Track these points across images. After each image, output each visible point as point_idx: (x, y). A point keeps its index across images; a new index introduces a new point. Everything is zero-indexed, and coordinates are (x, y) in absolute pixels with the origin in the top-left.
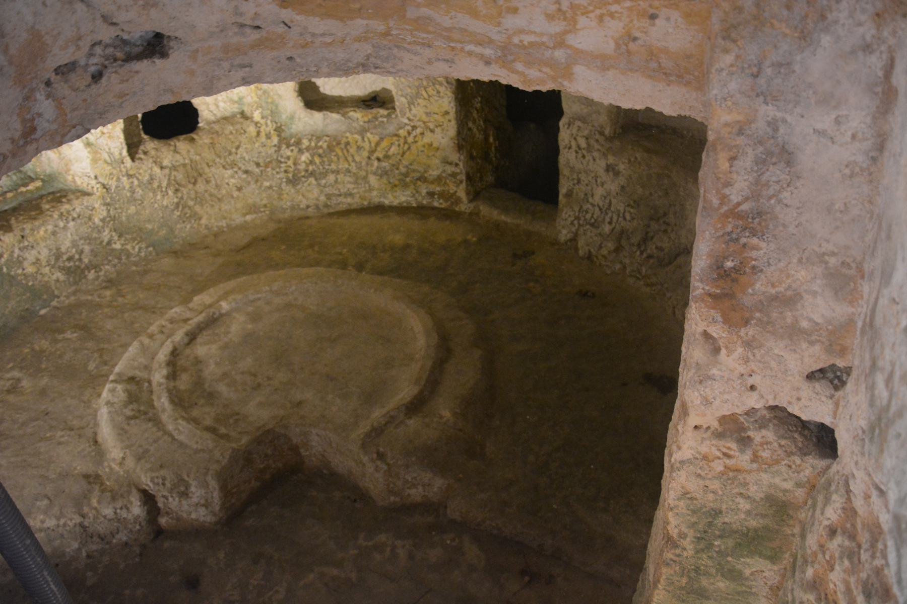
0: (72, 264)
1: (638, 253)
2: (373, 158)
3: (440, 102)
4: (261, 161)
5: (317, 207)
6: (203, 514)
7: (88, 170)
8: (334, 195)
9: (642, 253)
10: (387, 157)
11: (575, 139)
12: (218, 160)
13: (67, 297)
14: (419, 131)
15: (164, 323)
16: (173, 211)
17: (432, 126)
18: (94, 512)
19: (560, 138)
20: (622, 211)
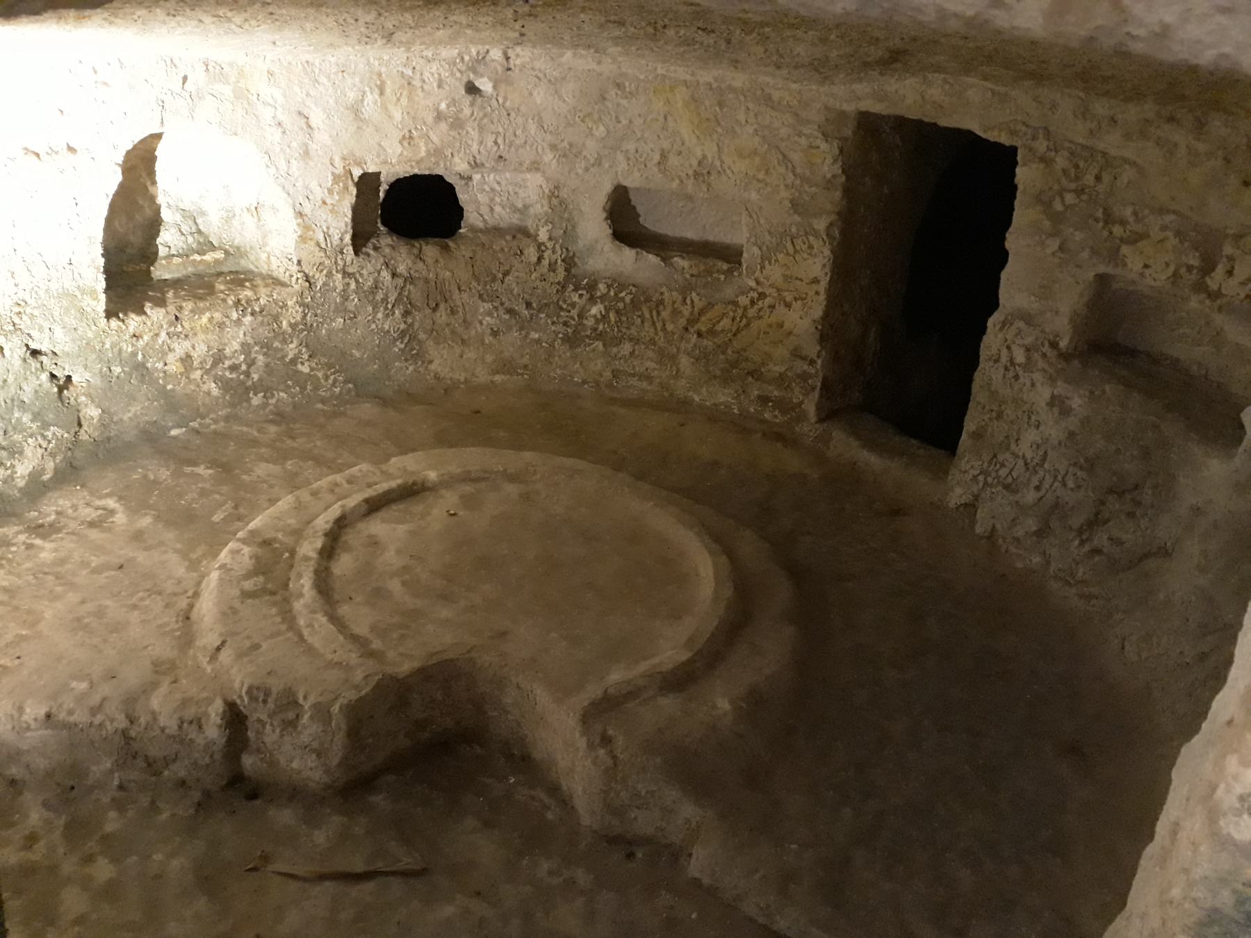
0: (234, 376)
1: (1077, 542)
3: (810, 262)
6: (310, 764)
7: (291, 251)
9: (1082, 543)
10: (712, 332)
11: (1008, 348)
12: (474, 284)
13: (215, 421)
14: (768, 301)
16: (395, 340)
20: (1063, 473)
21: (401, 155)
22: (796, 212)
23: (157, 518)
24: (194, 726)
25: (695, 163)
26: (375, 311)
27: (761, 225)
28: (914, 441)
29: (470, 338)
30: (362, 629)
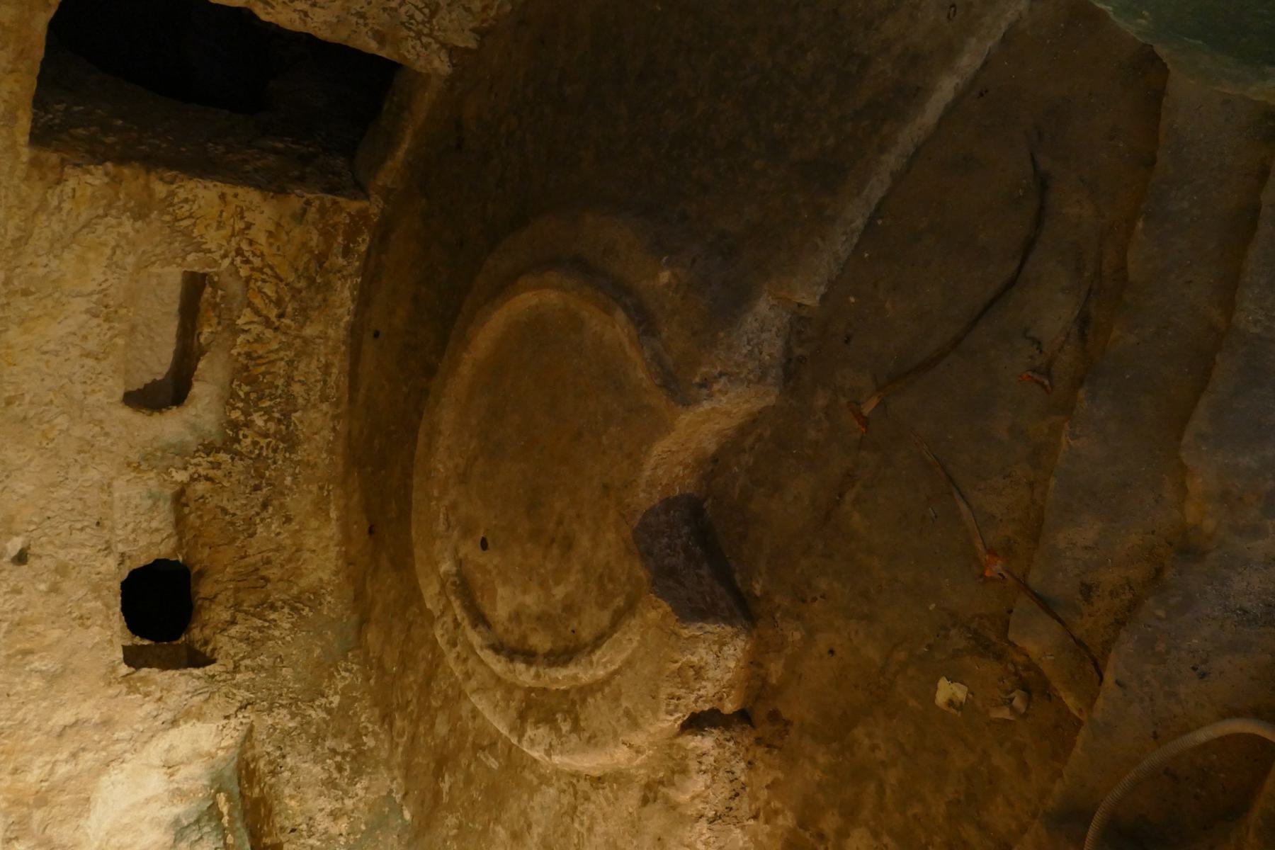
0: (347, 767)
2: (277, 324)
4: (252, 482)
5: (334, 417)
6: (732, 652)
7: (214, 727)
8: (323, 390)
10: (279, 302)
12: (238, 543)
14: (245, 246)
15: (453, 655)
16: (301, 617)
17: (240, 225)
18: (697, 801)
19: (289, 27)
21: (101, 626)
22: (147, 216)
23: (497, 820)
24: (704, 759)
25: (95, 321)
26: (273, 638)
27: (163, 253)
28: (386, 107)
29: (294, 544)
30: (605, 618)
